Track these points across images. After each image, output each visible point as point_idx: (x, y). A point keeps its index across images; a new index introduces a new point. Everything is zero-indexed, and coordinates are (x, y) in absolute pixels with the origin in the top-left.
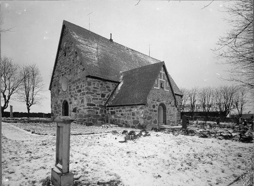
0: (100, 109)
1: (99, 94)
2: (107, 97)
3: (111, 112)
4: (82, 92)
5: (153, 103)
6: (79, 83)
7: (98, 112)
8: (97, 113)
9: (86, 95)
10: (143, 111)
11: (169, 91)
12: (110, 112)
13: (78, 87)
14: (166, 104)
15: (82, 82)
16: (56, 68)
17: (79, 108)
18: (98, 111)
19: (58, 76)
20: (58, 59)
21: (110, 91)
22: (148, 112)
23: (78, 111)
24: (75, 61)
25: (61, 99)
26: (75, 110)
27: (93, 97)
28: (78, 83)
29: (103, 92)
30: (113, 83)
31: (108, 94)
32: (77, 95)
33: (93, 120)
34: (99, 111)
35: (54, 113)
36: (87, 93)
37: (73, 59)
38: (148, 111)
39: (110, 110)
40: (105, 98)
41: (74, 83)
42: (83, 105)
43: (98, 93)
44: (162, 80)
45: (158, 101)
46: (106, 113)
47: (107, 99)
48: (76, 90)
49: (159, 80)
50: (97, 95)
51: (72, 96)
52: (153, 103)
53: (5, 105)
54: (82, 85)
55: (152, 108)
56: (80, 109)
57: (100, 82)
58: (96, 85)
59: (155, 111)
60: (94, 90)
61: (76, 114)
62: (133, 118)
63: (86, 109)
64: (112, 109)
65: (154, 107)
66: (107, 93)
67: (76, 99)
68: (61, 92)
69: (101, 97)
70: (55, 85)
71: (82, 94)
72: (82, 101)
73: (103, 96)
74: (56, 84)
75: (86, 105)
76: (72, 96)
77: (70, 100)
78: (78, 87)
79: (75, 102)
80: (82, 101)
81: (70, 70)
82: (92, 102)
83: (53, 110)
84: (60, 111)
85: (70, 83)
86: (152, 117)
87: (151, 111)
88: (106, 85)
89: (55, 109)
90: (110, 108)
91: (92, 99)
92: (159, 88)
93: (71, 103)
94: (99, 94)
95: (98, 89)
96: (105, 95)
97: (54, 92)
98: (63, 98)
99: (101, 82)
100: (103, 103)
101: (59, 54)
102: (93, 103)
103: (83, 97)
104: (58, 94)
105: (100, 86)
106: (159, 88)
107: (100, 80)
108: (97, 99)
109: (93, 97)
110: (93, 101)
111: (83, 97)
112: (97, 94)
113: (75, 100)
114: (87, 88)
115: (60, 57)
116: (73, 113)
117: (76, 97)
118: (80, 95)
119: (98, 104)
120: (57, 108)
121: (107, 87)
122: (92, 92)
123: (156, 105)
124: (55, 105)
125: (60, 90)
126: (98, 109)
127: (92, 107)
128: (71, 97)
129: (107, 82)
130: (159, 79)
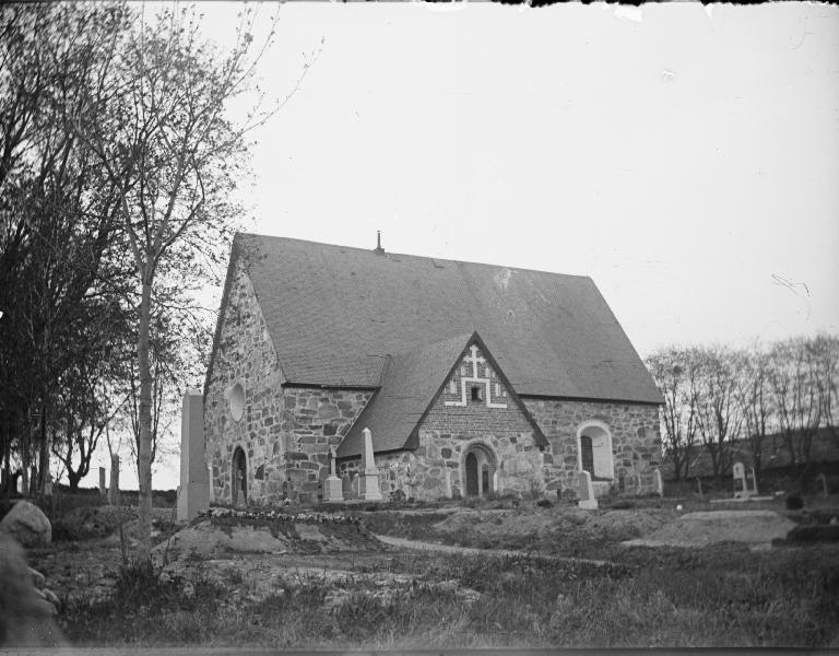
4: (275, 423)
11: (505, 406)
13: (265, 410)
14: (495, 443)
15: (274, 399)
17: (269, 466)
18: (314, 472)
22: (426, 469)
23: (267, 475)
26: (260, 474)
27: (300, 436)
29: (328, 422)
31: (344, 425)
33: (301, 496)
36: (284, 426)
39: (347, 469)
41: (257, 399)
43: (314, 424)
44: (476, 379)
45: (461, 438)
48: (263, 419)
49: (463, 383)
51: (253, 436)
53: (81, 467)
55: (440, 457)
56: (271, 470)
59: (451, 465)
60: (303, 418)
61: (263, 484)
62: (393, 486)
64: (351, 466)
65: (447, 453)
67: (262, 442)
69: (322, 434)
70: (214, 404)
72: (276, 449)
73: (329, 430)
75: (282, 458)
76: (253, 436)
77: (249, 445)
78: (265, 410)
79: (259, 452)
80: (276, 449)
81: (250, 364)
82: (297, 450)
84: (227, 479)
85: (249, 398)
87: (435, 465)
90: (347, 463)
92: (464, 403)
93: (334, 397)
96: (336, 427)
104: (222, 430)
105: (320, 404)
107: (318, 391)
109: (300, 436)
112: (312, 428)
114: (285, 415)
116: (256, 481)
120: (220, 468)
121: (342, 406)
123: (454, 450)
125: (227, 416)
126: (317, 467)
127: (297, 462)
128: (252, 438)
129: (340, 393)
130: (464, 380)
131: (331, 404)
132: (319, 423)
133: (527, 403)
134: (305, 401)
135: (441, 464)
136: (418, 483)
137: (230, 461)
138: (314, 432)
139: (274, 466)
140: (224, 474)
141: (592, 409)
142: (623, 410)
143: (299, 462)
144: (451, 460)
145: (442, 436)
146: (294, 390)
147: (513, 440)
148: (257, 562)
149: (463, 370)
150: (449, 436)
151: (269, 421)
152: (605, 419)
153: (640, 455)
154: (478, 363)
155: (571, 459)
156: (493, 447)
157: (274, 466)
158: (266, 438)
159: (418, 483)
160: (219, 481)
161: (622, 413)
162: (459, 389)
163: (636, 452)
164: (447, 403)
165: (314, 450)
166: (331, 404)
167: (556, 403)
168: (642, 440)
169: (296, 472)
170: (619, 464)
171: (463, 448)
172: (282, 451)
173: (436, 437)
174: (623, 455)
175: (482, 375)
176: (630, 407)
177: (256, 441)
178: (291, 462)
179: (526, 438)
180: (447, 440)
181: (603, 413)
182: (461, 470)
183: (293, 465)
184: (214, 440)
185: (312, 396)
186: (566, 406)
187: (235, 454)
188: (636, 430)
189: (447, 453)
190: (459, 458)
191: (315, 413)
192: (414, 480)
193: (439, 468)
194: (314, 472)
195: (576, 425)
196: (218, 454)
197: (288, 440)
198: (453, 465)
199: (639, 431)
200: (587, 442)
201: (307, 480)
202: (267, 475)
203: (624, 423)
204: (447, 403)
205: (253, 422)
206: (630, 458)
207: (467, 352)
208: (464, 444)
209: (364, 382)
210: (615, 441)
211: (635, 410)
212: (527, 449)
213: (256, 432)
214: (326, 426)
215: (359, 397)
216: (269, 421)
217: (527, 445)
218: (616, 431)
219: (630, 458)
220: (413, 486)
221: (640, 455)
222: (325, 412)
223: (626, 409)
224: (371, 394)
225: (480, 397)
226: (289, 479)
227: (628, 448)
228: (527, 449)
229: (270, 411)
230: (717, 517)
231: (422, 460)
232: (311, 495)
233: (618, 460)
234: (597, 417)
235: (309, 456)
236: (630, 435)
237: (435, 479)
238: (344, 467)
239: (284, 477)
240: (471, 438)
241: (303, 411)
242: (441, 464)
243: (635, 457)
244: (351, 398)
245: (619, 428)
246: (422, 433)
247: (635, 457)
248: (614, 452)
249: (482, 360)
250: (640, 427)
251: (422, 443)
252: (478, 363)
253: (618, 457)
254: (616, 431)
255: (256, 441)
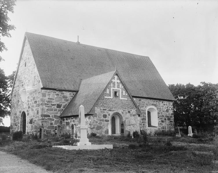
0: (55, 119)
1: (54, 105)
2: (64, 107)
3: (66, 122)
4: (38, 103)
5: (104, 112)
6: (36, 94)
7: (52, 123)
8: (52, 124)
9: (40, 106)
10: (91, 120)
11: (126, 99)
12: (65, 123)
13: (34, 98)
14: (123, 113)
15: (38, 94)
16: (17, 77)
17: (35, 119)
18: (53, 122)
19: (18, 86)
20: (20, 68)
21: (67, 100)
23: (34, 122)
24: (33, 72)
25: (20, 110)
26: (31, 122)
27: (48, 108)
28: (35, 95)
29: (58, 103)
30: (70, 93)
31: (64, 104)
32: (33, 106)
34: (53, 122)
35: (13, 125)
36: (42, 104)
37: (31, 70)
38: (96, 120)
39: (65, 121)
40: (61, 108)
42: (38, 116)
43: (53, 104)
44: (116, 88)
45: (110, 110)
46: (62, 124)
47: (64, 109)
50: (52, 106)
52: (104, 112)
54: (38, 96)
55: (102, 118)
56: (35, 121)
57: (55, 92)
58: (51, 96)
59: (106, 121)
61: (32, 126)
63: (40, 120)
64: (67, 120)
65: (105, 116)
66: (64, 103)
68: (20, 102)
69: (56, 108)
71: (37, 105)
72: (38, 113)
73: (59, 106)
74: (16, 94)
75: (40, 116)
80: (38, 113)
81: (29, 81)
82: (46, 113)
83: (13, 122)
86: (102, 127)
88: (62, 95)
89: (15, 121)
91: (47, 110)
92: (112, 97)
93: (28, 114)
94: (54, 105)
95: (53, 99)
96: (61, 105)
97: (14, 103)
98: (22, 109)
99: (57, 92)
100: (59, 113)
101: (20, 64)
102: (48, 114)
103: (38, 108)
105: (56, 96)
106: (112, 97)
107: (55, 91)
108: (52, 110)
110: (47, 112)
111: (38, 108)
112: (52, 105)
113: (32, 111)
114: (42, 100)
115: (22, 66)
117: (32, 108)
118: (36, 107)
119: (53, 115)
120: (16, 119)
121: (64, 97)
122: (46, 102)
123: (107, 115)
124: (14, 117)
127: (46, 118)
129: (64, 92)
130: (112, 88)
131: (60, 96)
132: (55, 103)
133: (134, 99)
134: (50, 95)
135: (103, 120)
136: (94, 128)
137: (20, 117)
138: (53, 107)
139: (37, 119)
140: (17, 121)
141: (151, 102)
142: (161, 103)
143: (47, 118)
144: (106, 119)
145: (103, 110)
146: (46, 91)
147: (129, 112)
148: (181, 152)
149: (112, 85)
150: (106, 110)
151: (36, 102)
152: (155, 105)
153: (167, 118)
154: (117, 83)
155: (144, 119)
156: (26, 115)
157: (37, 119)
158: (34, 109)
159: (94, 128)
160: (15, 124)
161: (161, 104)
162: (110, 91)
163: (165, 117)
164: (106, 97)
165: (53, 113)
166: (60, 96)
167: (140, 99)
168: (167, 113)
169: (46, 121)
170: (160, 122)
171: (111, 114)
172: (40, 114)
173: (101, 110)
174: (161, 118)
175: (118, 87)
176: (164, 102)
177: (30, 109)
178: (43, 118)
179: (134, 111)
180: (105, 111)
181: (155, 103)
182: (110, 122)
183: (44, 119)
184: (15, 109)
185: (52, 93)
186: (143, 100)
187: (22, 114)
188: (165, 109)
189: (105, 116)
190: (109, 118)
191: (53, 99)
192: (92, 126)
193: (102, 122)
194: (53, 122)
195: (146, 107)
196: (16, 114)
197: (43, 109)
198: (107, 121)
199: (167, 110)
200: (149, 113)
201: (49, 125)
202: (34, 122)
203: (162, 107)
204: (106, 97)
205: (30, 103)
206: (163, 120)
207: (114, 78)
208: (111, 113)
209: (72, 89)
210: (158, 113)
211: (165, 102)
212: (134, 115)
213: (30, 106)
214: (58, 105)
215: (70, 94)
216: (36, 102)
217: (133, 114)
218: (159, 110)
219: (163, 120)
220: (92, 129)
221: (167, 118)
222: (57, 99)
223: (163, 102)
224: (75, 93)
225: (117, 95)
226: (43, 124)
227: (163, 116)
228: (134, 115)
229: (36, 98)
230: (61, 147)
231: (95, 119)
232: (51, 130)
233: (160, 120)
234: (153, 105)
235: (51, 116)
236: (164, 112)
237: (100, 126)
238: (64, 120)
239: (41, 124)
240: (114, 110)
241: (49, 98)
242: (103, 120)
243: (165, 119)
244: (67, 94)
245: (160, 109)
246: (96, 108)
247: (165, 119)
248: (158, 117)
249: (119, 81)
250: (167, 109)
251: (96, 112)
252: (117, 83)
253: (160, 119)
254: (159, 110)
255: (30, 109)
